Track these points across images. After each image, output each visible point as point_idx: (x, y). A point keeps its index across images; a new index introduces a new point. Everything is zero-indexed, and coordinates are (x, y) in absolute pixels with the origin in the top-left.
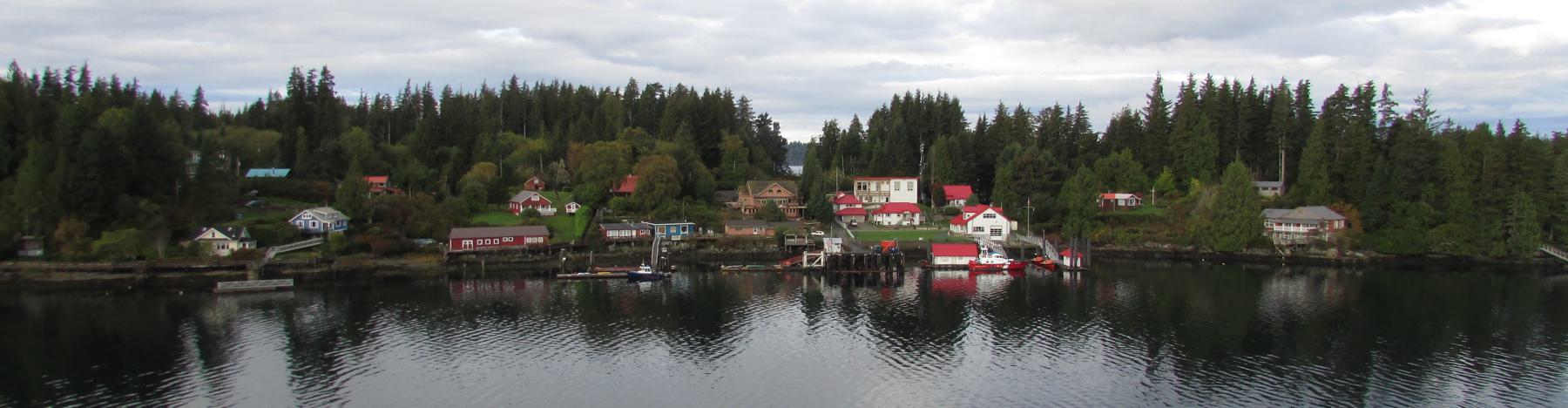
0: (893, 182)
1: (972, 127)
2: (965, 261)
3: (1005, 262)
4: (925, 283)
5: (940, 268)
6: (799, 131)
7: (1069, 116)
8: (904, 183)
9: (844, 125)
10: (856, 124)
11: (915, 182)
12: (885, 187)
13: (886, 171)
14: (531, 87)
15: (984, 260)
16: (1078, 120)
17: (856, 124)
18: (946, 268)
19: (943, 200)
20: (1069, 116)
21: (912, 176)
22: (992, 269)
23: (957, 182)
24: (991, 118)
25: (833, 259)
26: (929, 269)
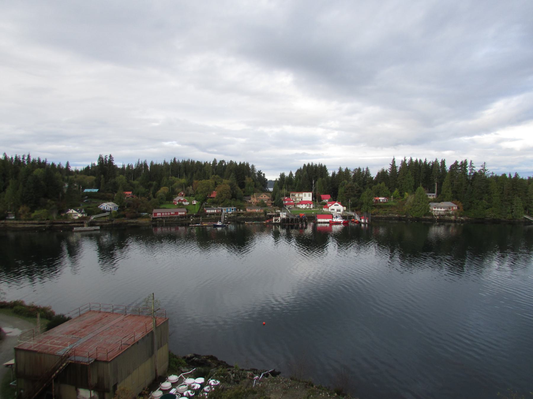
0: (303, 193)
1: (331, 175)
2: (328, 220)
4: (314, 228)
5: (320, 223)
7: (363, 171)
8: (307, 194)
9: (287, 174)
10: (291, 174)
11: (311, 194)
12: (301, 195)
15: (334, 220)
16: (367, 173)
17: (291, 174)
18: (322, 223)
20: (363, 171)
22: (337, 223)
23: (325, 194)
24: (337, 172)
26: (316, 223)
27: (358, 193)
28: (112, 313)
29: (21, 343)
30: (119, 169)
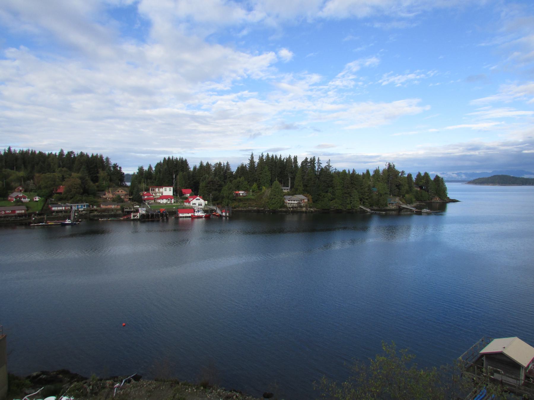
0: (164, 188)
1: (192, 169)
2: (190, 215)
5: (181, 217)
7: (224, 166)
8: (168, 188)
9: (146, 168)
10: (150, 167)
11: (172, 188)
12: (161, 190)
15: (196, 214)
16: (227, 167)
17: (150, 167)
18: (183, 217)
20: (224, 166)
21: (171, 186)
23: (186, 188)
27: (219, 187)
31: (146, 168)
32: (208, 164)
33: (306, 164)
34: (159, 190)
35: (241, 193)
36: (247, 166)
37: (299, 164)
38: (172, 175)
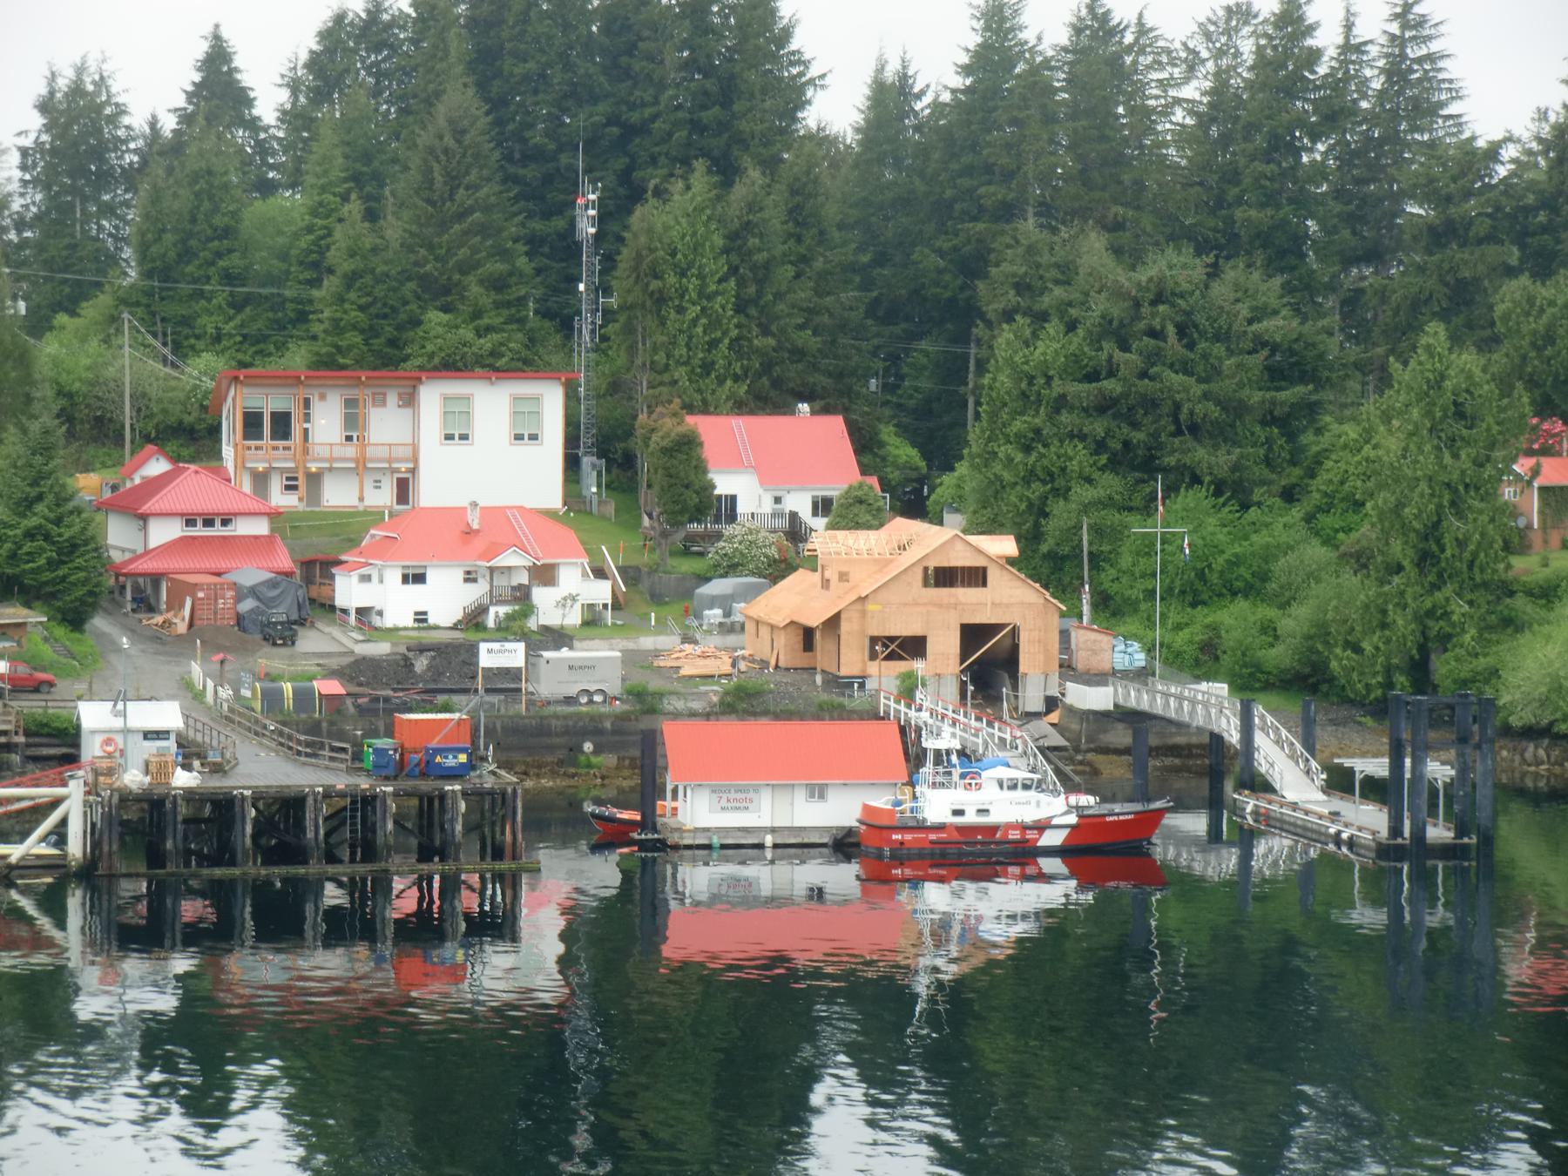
0: (432, 395)
1: (835, 110)
2: (841, 810)
3: (1055, 810)
4: (616, 935)
5: (705, 849)
6: (836, 423)
7: (1351, 49)
8: (492, 403)
9: (152, 96)
10: (218, 86)
11: (551, 401)
12: (386, 424)
13: (386, 346)
14: (959, 82)
15: (938, 805)
16: (1397, 71)
17: (218, 86)
18: (742, 847)
19: (696, 508)
20: (1351, 49)
21: (525, 365)
22: (982, 854)
23: (770, 395)
24: (940, 74)
25: (140, 825)
26: (650, 852)
27: (1277, 375)
28: (733, 905)
29: (1075, 772)
30: (807, 1099)
31: (152, 96)
32: (1096, 31)
33: (1282, 146)
34: (353, 422)
35: (331, 1122)
36: (1059, 79)
37: (363, 15)
38: (550, 198)
